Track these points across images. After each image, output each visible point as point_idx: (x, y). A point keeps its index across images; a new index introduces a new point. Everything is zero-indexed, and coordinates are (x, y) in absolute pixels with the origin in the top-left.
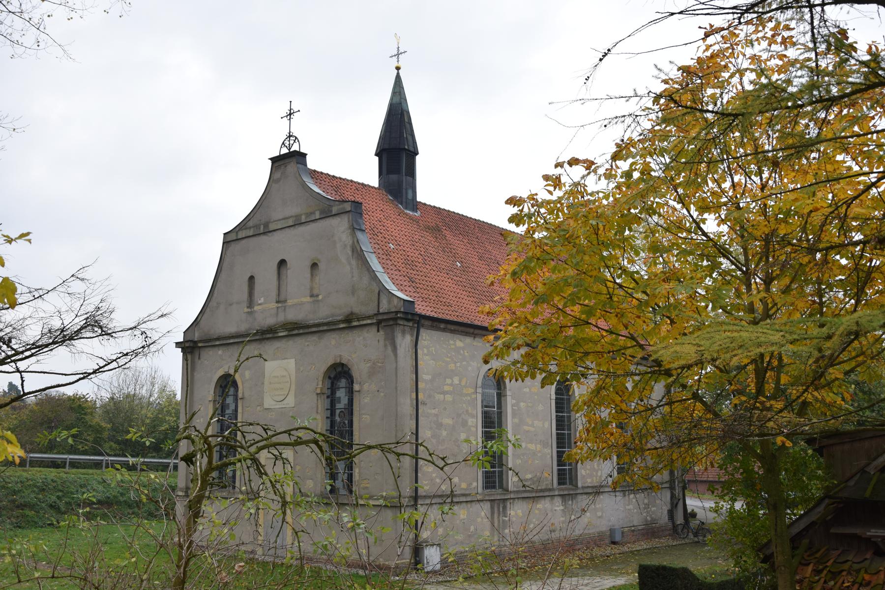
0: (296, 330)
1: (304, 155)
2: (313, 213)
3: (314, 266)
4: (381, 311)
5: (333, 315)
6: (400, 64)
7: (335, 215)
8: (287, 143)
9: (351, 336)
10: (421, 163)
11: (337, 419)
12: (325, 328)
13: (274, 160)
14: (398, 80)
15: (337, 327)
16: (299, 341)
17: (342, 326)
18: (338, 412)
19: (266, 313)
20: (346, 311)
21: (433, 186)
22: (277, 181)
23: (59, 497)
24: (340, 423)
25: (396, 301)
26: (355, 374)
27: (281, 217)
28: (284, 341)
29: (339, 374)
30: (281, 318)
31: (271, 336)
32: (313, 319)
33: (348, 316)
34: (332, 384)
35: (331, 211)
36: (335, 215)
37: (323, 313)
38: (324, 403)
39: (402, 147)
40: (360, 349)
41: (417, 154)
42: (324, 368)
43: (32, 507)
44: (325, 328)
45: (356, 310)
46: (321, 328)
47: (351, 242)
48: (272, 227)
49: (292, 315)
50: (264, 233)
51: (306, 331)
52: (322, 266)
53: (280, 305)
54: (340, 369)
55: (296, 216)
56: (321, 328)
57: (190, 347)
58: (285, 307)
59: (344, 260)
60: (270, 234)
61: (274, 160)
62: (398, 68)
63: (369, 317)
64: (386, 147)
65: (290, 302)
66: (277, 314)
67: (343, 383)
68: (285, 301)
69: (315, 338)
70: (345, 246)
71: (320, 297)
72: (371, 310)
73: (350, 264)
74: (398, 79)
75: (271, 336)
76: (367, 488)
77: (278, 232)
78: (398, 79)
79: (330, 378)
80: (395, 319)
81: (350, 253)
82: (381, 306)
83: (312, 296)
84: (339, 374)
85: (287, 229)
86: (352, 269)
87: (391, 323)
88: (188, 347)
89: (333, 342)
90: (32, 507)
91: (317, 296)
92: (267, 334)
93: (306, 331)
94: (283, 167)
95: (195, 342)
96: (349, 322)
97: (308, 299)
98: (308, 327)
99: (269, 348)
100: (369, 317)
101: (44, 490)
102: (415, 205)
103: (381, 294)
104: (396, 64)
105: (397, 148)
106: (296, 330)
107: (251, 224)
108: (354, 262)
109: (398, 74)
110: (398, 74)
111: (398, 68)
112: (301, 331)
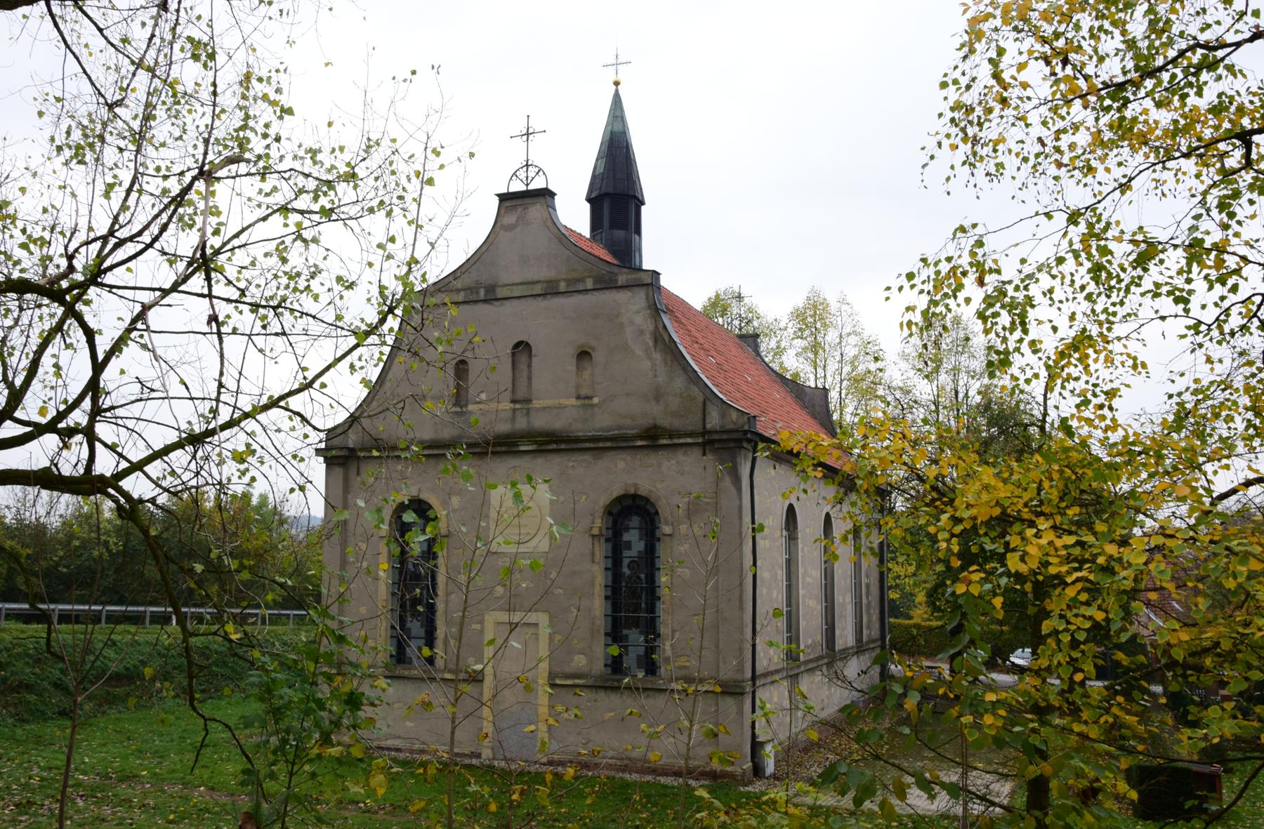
0: (551, 443)
1: (552, 195)
2: (582, 280)
3: (584, 355)
4: (708, 426)
5: (620, 428)
6: (620, 78)
7: (621, 287)
8: (522, 174)
9: (652, 459)
10: (649, 216)
11: (626, 571)
12: (609, 444)
13: (504, 198)
14: (617, 101)
15: (631, 444)
16: (557, 460)
17: (639, 443)
18: (626, 562)
19: (490, 411)
20: (645, 422)
21: (658, 247)
22: (510, 228)
23: (62, 671)
24: (630, 577)
25: (734, 415)
26: (664, 511)
27: (518, 280)
28: (527, 458)
29: (632, 513)
30: (521, 424)
31: (503, 449)
32: (579, 429)
33: (648, 429)
34: (615, 522)
35: (616, 281)
36: (621, 287)
37: (602, 422)
38: (601, 550)
39: (631, 193)
40: (672, 479)
41: (643, 203)
42: (604, 500)
43: (29, 688)
44: (609, 444)
45: (665, 422)
46: (601, 445)
47: (651, 328)
48: (501, 293)
49: (540, 422)
50: (485, 301)
51: (574, 446)
52: (598, 356)
53: (518, 406)
54: (630, 502)
55: (549, 282)
56: (601, 445)
57: (344, 452)
58: (528, 410)
59: (638, 350)
60: (497, 303)
61: (504, 198)
62: (617, 84)
63: (691, 434)
64: (610, 190)
65: (536, 404)
66: (513, 419)
67: (635, 521)
68: (529, 401)
69: (587, 457)
70: (642, 332)
71: (596, 400)
72: (691, 422)
73: (650, 357)
74: (617, 97)
75: (503, 449)
76: (685, 667)
77: (515, 302)
78: (617, 97)
79: (610, 513)
80: (739, 441)
81: (651, 343)
82: (708, 420)
83: (578, 397)
84: (632, 513)
85: (530, 299)
86: (654, 365)
87: (732, 445)
88: (333, 457)
89: (621, 465)
90: (29, 688)
91: (590, 398)
92: (503, 446)
93: (574, 446)
94: (520, 209)
95: (352, 450)
96: (653, 439)
97: (573, 401)
98: (577, 440)
99: (501, 467)
100: (690, 435)
101: (39, 660)
102: (640, 270)
103: (708, 403)
104: (614, 78)
105: (617, 194)
106: (551, 443)
107: (458, 284)
108: (658, 356)
109: (617, 91)
110: (617, 91)
111: (617, 84)
112: (563, 446)
